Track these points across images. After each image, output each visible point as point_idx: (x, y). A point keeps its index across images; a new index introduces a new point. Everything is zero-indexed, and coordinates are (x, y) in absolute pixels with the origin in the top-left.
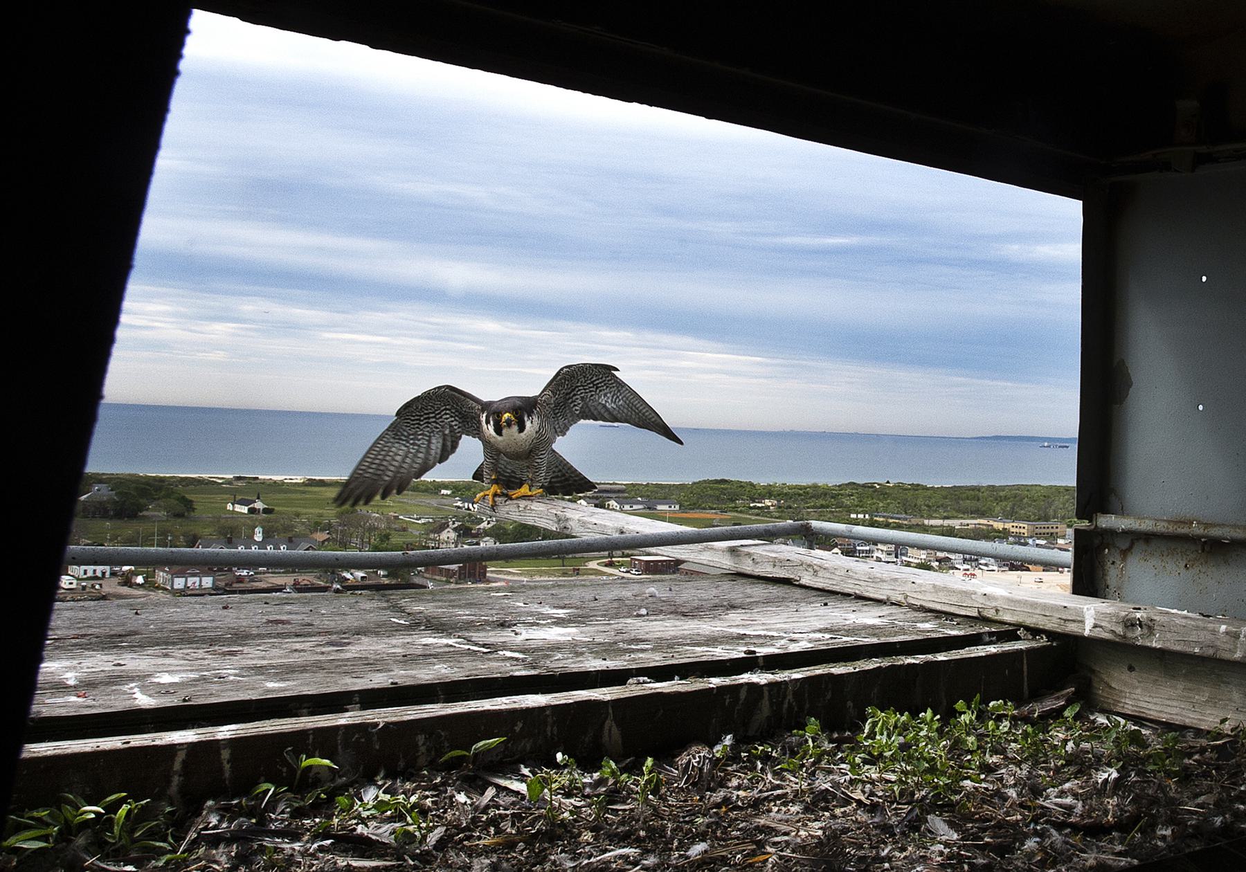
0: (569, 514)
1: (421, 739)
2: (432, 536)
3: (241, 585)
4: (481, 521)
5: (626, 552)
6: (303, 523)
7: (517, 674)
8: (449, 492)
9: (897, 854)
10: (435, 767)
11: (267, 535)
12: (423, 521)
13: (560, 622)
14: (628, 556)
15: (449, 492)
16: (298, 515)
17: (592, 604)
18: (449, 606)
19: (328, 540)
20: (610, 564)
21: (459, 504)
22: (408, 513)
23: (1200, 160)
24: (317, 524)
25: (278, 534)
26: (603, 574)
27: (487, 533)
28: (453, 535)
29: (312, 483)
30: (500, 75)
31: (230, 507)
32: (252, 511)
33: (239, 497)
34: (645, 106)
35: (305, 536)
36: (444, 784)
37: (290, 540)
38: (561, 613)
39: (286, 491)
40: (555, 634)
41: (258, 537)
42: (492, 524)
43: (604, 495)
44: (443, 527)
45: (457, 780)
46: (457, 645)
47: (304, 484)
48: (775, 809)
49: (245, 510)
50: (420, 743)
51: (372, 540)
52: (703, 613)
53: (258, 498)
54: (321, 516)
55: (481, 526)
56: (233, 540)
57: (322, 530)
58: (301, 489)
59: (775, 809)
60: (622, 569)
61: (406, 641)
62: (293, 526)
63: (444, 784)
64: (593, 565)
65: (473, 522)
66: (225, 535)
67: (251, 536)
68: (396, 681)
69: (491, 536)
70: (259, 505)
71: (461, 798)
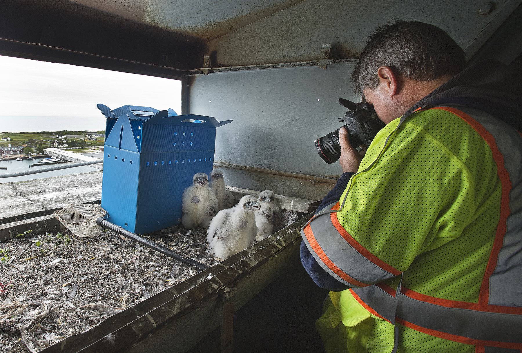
0: (65, 155)
1: (10, 232)
2: (52, 144)
3: (7, 158)
4: (63, 141)
5: (98, 147)
6: (20, 143)
7: (38, 211)
8: (55, 134)
9: (127, 255)
10: (14, 238)
11: (12, 145)
12: (49, 141)
13: (55, 190)
14: (98, 147)
15: (55, 134)
16: (19, 141)
17: (65, 183)
18: (28, 186)
19: (27, 146)
20: (94, 149)
21: (58, 137)
22: (45, 139)
23: (210, 71)
24: (24, 143)
25: (15, 145)
26: (93, 152)
27: (65, 143)
28: (57, 144)
29: (21, 133)
30: (12, 57)
31: (2, 139)
32: (7, 140)
33: (4, 137)
34: (58, 63)
35: (21, 146)
36: (17, 243)
37: (18, 147)
38: (56, 187)
39: (15, 135)
40: (52, 195)
41: (10, 146)
42: (66, 141)
43: (92, 134)
44: (54, 142)
45: (20, 242)
46: (25, 201)
47: (19, 133)
48: (101, 242)
49: (6, 140)
50: (10, 233)
51: (37, 146)
52: (92, 185)
53: (9, 137)
54: (24, 141)
55: (63, 142)
56: (4, 147)
57: (25, 144)
58: (19, 134)
59: (101, 242)
60: (97, 150)
61: (13, 200)
62: (18, 143)
63: (17, 243)
64: (90, 150)
65: (61, 141)
66: (1, 146)
67: (8, 146)
68: (4, 217)
69: (66, 144)
70: (9, 139)
71: (21, 247)
